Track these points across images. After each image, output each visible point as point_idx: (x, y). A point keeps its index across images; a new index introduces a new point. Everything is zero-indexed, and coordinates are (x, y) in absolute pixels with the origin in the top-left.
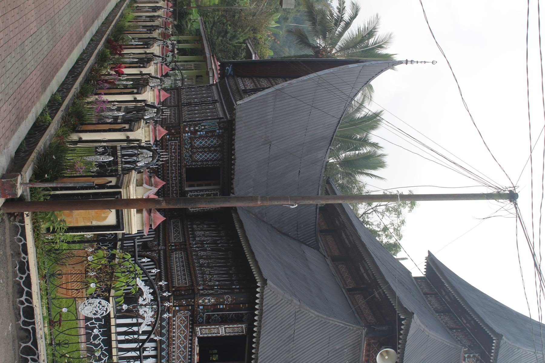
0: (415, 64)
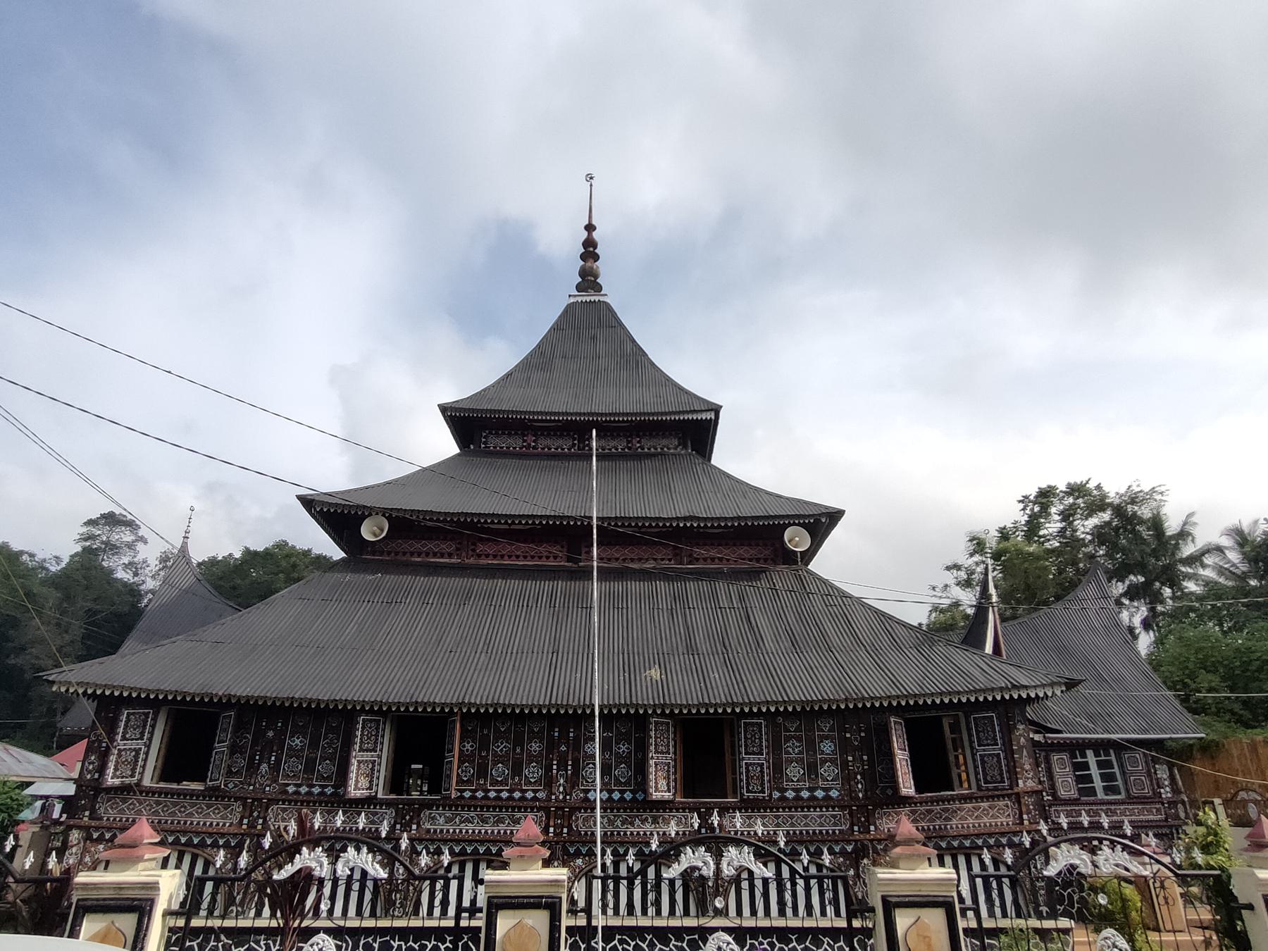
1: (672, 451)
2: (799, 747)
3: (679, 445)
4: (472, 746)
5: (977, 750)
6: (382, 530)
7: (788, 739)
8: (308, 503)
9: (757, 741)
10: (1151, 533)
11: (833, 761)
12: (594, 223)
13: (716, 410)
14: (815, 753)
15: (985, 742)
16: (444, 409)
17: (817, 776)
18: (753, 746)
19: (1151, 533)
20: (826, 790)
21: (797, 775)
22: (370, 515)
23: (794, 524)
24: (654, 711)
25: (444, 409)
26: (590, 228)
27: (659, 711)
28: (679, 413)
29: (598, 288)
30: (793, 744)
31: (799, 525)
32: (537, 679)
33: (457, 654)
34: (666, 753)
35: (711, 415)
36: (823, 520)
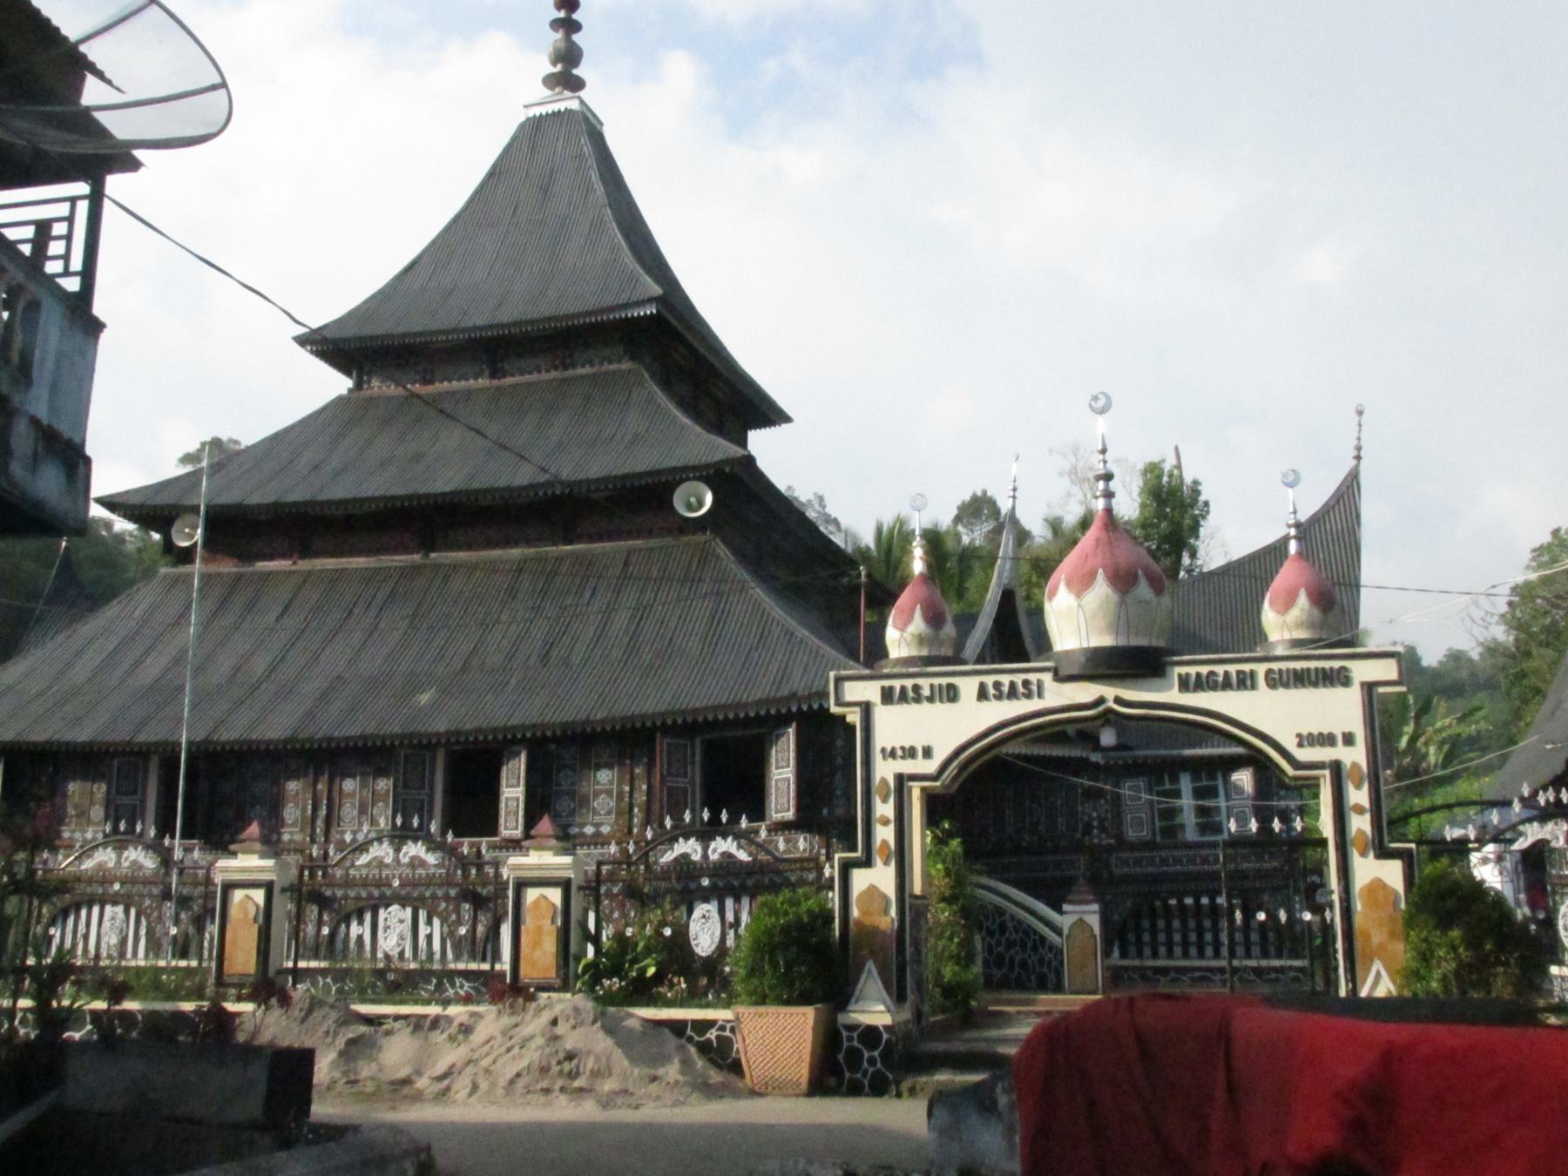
0: (1363, 454)
11: (609, 793)
20: (597, 825)
29: (576, 84)
31: (695, 478)
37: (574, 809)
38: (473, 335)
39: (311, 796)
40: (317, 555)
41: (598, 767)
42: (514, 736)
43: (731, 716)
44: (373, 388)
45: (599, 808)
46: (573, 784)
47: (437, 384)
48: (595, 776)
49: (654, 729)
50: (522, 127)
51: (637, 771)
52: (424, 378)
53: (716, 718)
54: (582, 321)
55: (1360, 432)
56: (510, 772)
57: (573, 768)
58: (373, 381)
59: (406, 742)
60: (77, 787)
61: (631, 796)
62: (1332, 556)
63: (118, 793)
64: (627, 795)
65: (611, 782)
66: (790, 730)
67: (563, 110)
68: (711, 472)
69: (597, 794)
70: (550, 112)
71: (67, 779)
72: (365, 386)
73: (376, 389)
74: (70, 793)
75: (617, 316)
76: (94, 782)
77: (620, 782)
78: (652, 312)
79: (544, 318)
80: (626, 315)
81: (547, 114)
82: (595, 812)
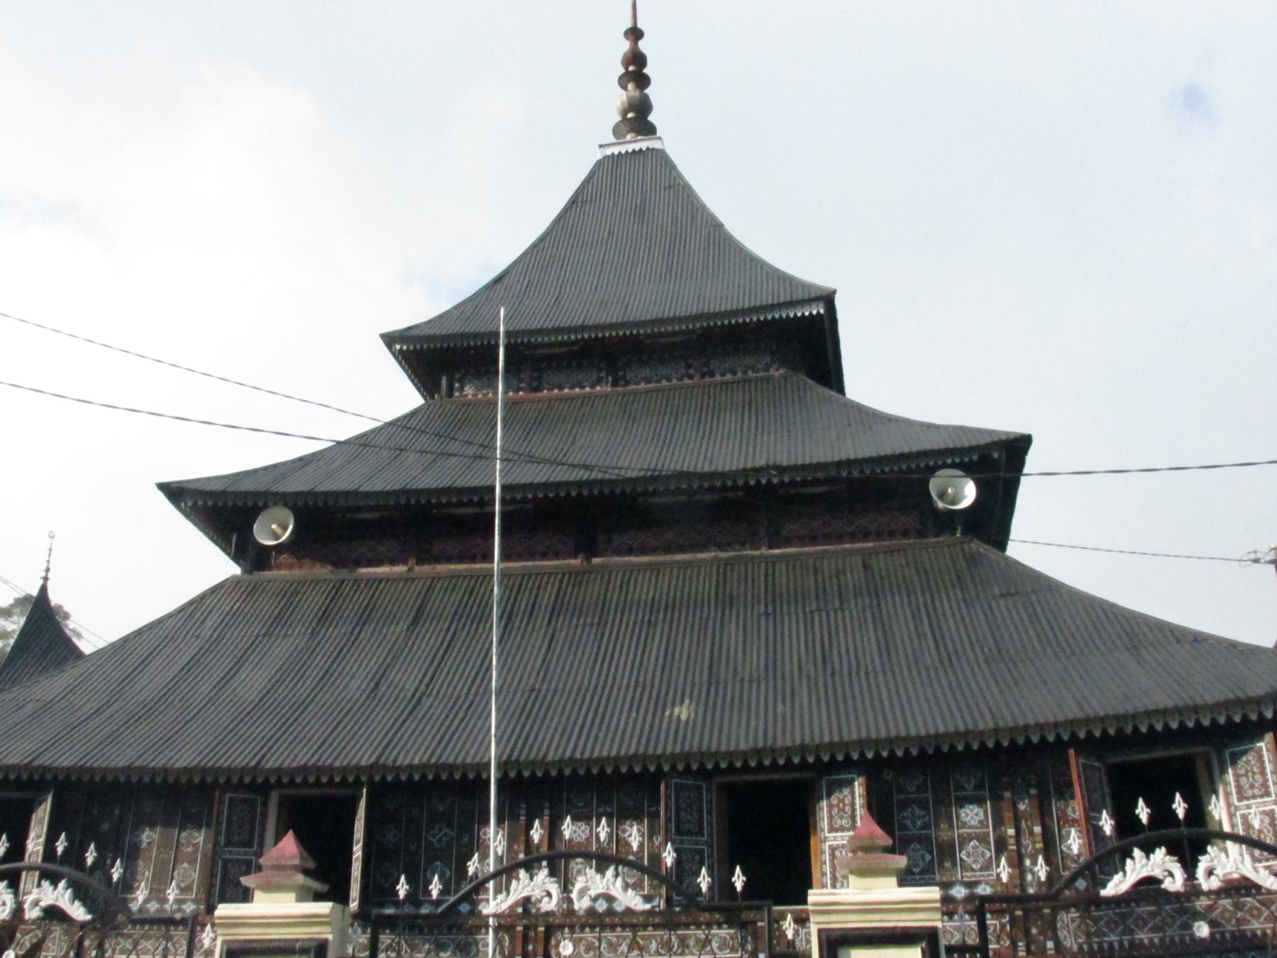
1: (761, 374)
2: (924, 817)
3: (773, 362)
4: (395, 836)
5: (1237, 808)
6: (285, 528)
7: (903, 805)
8: (175, 492)
9: (847, 808)
10: (444, 381)
11: (983, 839)
12: (639, 26)
13: (828, 299)
14: (951, 826)
15: (1250, 793)
16: (390, 339)
17: (954, 864)
18: (841, 818)
19: (444, 381)
20: (971, 885)
21: (921, 863)
22: (266, 506)
23: (945, 466)
24: (674, 767)
25: (390, 339)
26: (635, 34)
27: (680, 767)
28: (772, 307)
29: (649, 130)
30: (913, 814)
31: (954, 466)
32: (519, 736)
33: (375, 703)
34: (696, 834)
35: (818, 309)
36: (996, 455)
37: (932, 861)
38: (432, 346)
39: (522, 847)
40: (437, 560)
41: (962, 802)
42: (848, 758)
43: (1174, 725)
44: (467, 395)
45: (969, 861)
46: (926, 826)
47: (545, 391)
48: (958, 816)
49: (1061, 746)
50: (599, 164)
51: (1022, 807)
52: (529, 384)
53: (1229, 720)
54: (726, 322)
55: (50, 555)
56: (835, 810)
57: (923, 805)
58: (466, 389)
59: (680, 767)
60: (156, 836)
61: (1018, 843)
62: (353, 752)
63: (229, 843)
64: (1012, 841)
65: (983, 824)
66: (1262, 744)
67: (644, 149)
68: (975, 458)
69: (964, 840)
70: (630, 151)
71: (138, 827)
72: (457, 394)
73: (470, 397)
74: (144, 845)
75: (777, 316)
76: (182, 829)
77: (998, 822)
78: (818, 312)
79: (524, 331)
80: (788, 315)
81: (627, 152)
82: (965, 867)
